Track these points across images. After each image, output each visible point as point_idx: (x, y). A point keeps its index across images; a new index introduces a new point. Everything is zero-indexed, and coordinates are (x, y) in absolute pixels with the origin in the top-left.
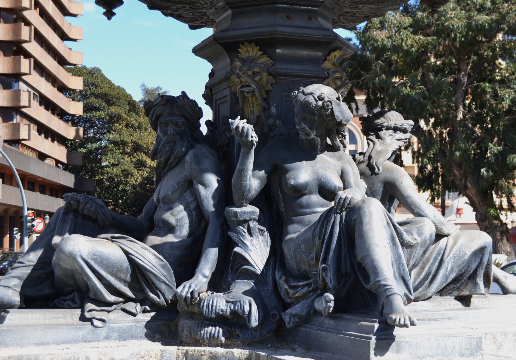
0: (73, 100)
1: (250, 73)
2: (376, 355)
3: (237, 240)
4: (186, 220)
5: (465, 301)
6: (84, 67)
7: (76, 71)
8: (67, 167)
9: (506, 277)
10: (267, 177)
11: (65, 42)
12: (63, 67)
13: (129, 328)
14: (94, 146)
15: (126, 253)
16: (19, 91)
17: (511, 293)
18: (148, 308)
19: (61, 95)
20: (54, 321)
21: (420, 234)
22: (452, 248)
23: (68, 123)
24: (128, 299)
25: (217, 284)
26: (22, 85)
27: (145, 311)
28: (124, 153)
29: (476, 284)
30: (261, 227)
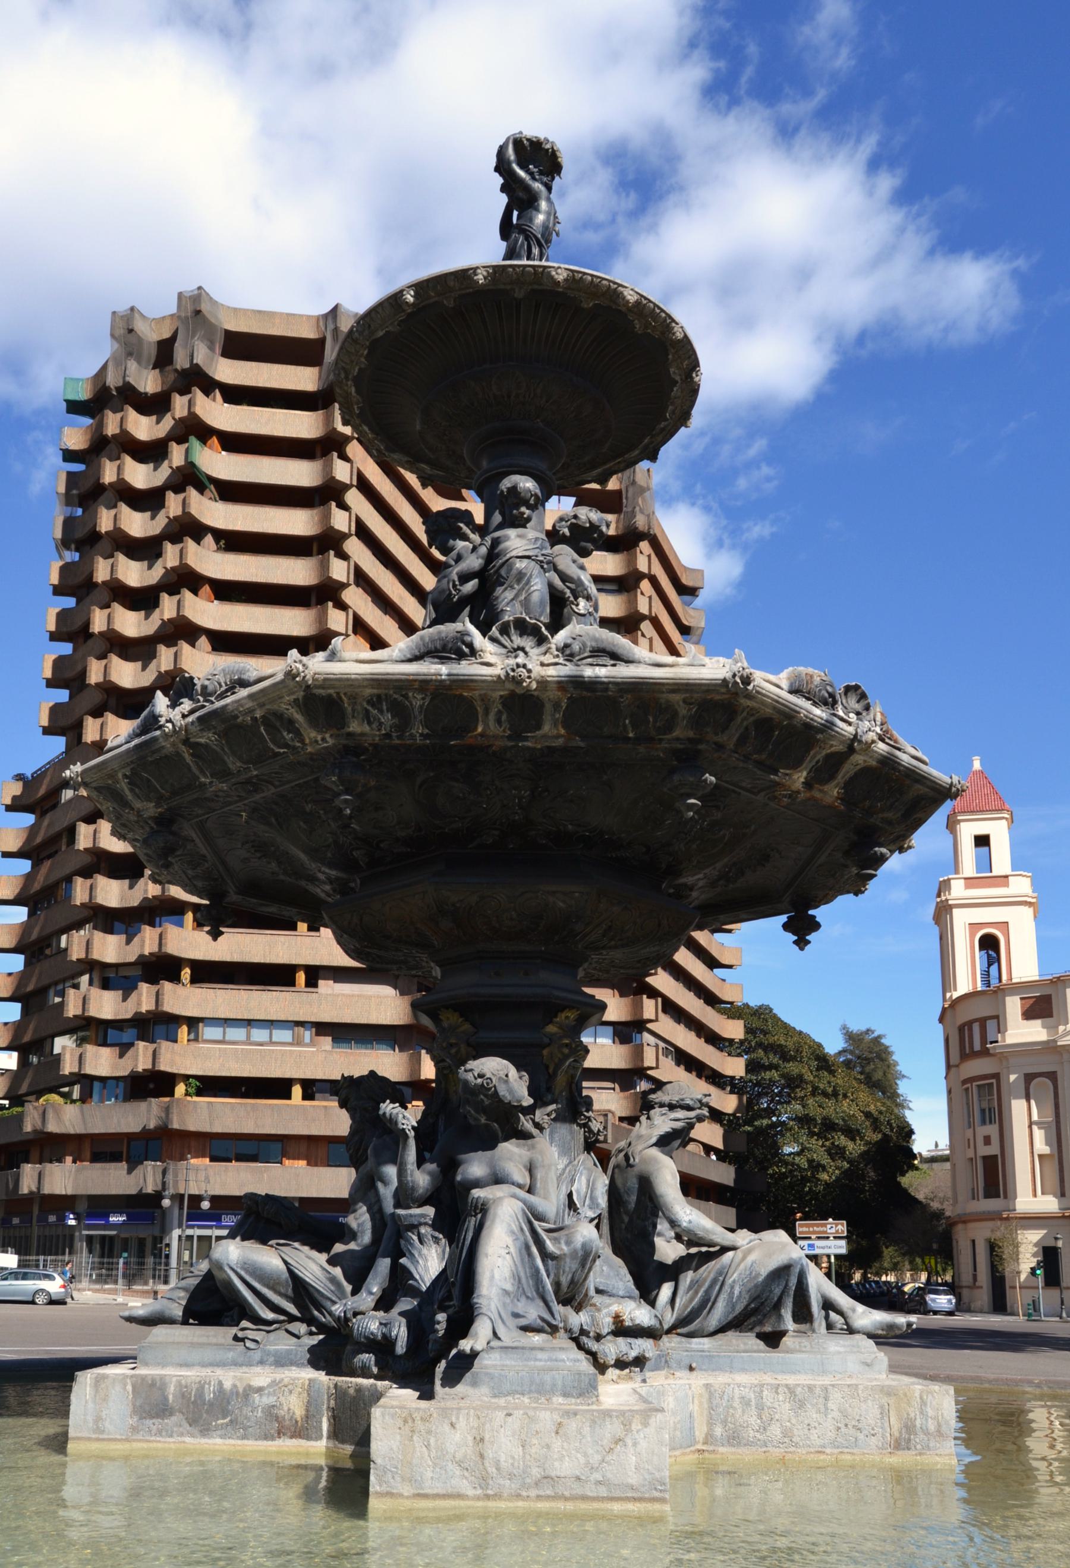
1: (444, 1045)
2: (443, 1386)
3: (405, 1249)
4: (368, 1225)
5: (773, 1340)
6: (747, 1005)
7: (733, 1011)
8: (723, 1156)
9: (854, 1310)
10: (441, 1171)
11: (715, 970)
12: (713, 1007)
13: (289, 1352)
14: (765, 1122)
15: (286, 1262)
16: (642, 1045)
17: (859, 1332)
18: (314, 1329)
21: (568, 1243)
22: (739, 1265)
23: (724, 1089)
24: (292, 1319)
25: (384, 1303)
26: (647, 1037)
27: (311, 1333)
28: (812, 1134)
29: (780, 1317)
30: (437, 1234)
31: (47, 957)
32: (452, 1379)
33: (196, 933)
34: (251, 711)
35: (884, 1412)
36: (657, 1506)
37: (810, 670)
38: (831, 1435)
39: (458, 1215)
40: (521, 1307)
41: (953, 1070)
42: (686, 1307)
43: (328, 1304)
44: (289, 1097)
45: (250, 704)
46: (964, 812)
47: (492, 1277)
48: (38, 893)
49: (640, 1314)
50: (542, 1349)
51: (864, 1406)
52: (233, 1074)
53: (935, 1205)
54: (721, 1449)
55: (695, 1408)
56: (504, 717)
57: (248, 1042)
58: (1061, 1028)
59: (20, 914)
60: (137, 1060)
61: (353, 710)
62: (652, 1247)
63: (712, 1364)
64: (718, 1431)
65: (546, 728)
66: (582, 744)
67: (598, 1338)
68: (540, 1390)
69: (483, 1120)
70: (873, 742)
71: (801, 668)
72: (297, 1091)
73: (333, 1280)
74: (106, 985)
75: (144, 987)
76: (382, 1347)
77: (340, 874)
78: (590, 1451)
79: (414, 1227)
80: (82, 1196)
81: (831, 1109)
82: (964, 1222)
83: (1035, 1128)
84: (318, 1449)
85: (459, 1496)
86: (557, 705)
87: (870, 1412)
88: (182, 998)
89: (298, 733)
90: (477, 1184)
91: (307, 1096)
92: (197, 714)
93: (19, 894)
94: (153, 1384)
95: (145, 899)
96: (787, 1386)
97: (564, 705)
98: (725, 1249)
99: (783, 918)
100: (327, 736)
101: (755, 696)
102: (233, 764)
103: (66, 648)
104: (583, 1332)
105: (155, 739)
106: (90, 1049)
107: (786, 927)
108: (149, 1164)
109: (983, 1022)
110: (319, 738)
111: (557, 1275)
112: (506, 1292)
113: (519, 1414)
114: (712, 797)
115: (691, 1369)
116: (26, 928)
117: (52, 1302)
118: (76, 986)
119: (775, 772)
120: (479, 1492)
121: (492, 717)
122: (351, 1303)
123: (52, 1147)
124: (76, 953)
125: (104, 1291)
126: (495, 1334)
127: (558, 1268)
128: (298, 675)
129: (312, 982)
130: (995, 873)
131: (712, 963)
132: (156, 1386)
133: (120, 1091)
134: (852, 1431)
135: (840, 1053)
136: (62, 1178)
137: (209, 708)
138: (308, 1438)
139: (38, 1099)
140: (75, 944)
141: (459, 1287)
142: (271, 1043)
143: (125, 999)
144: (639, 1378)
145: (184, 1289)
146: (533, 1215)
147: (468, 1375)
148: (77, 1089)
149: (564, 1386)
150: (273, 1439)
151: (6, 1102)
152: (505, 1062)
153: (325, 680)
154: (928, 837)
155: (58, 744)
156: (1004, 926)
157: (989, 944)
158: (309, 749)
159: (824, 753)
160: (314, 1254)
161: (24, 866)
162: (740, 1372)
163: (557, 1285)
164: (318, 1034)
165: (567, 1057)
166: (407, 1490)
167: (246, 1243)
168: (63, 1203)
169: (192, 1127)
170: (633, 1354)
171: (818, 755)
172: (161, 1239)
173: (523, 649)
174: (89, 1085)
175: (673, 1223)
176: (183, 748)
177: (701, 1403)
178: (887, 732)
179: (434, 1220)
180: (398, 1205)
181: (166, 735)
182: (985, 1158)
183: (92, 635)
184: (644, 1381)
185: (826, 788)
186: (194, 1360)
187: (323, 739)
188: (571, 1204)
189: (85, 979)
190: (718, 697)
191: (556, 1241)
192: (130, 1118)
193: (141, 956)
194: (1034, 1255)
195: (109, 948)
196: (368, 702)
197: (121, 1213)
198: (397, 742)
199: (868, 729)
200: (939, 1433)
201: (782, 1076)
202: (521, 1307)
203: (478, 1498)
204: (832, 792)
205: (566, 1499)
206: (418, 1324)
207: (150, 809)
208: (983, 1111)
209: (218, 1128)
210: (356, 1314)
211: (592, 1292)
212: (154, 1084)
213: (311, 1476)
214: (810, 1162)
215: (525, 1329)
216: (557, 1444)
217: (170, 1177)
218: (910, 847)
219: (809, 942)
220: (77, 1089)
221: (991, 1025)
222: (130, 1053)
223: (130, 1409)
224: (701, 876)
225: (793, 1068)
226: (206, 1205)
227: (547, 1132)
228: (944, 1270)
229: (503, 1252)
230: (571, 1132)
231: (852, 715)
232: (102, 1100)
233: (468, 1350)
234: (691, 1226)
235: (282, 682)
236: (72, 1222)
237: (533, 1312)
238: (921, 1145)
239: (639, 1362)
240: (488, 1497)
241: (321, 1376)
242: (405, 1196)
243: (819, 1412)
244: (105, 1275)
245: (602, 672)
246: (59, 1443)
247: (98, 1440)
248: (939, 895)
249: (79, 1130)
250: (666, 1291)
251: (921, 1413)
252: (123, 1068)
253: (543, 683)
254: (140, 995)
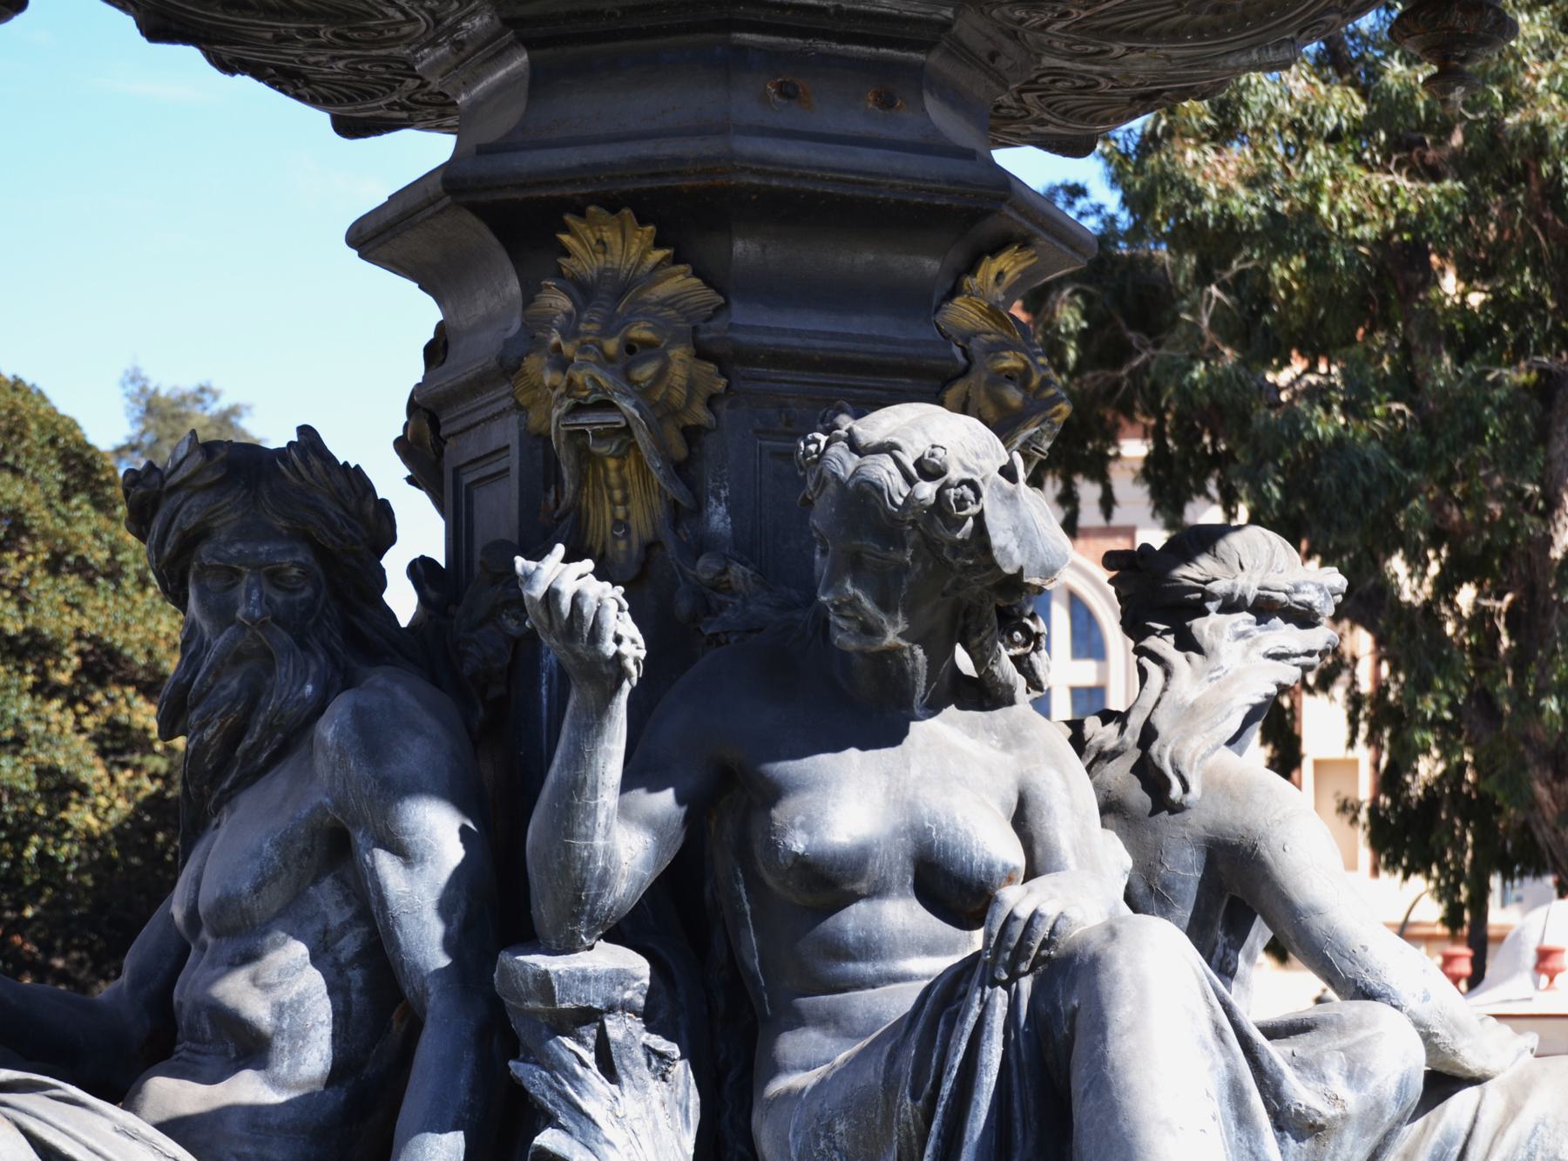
1: (612, 346)
3: (548, 1099)
4: (320, 1011)
10: (687, 818)
21: (1355, 1074)
28: (44, 689)
135: (119, 452)
179: (651, 995)
214: (44, 772)
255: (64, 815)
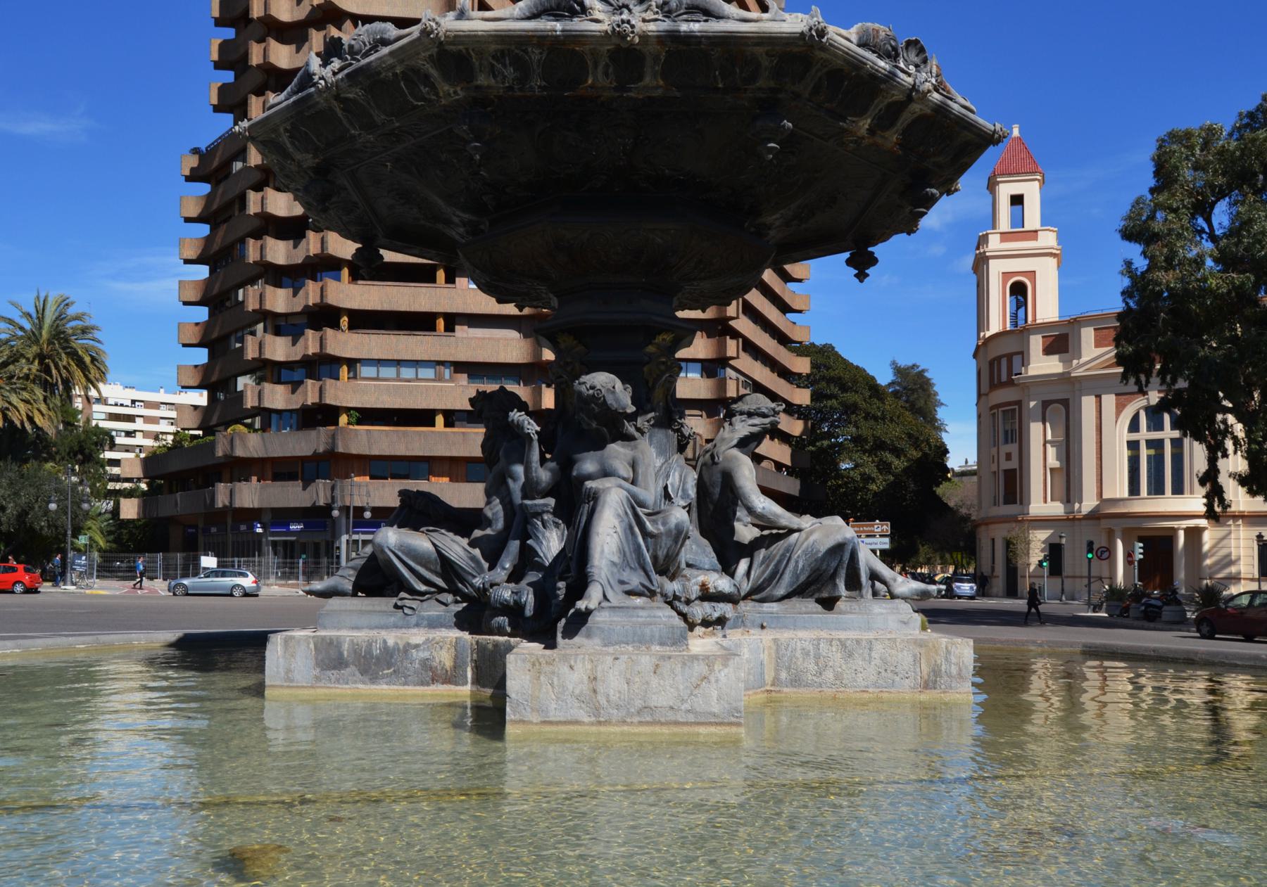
0: (798, 387)
2: (563, 638)
4: (501, 514)
5: (829, 604)
6: (813, 344)
7: (802, 350)
8: (792, 471)
9: (895, 580)
19: (782, 381)
20: (370, 608)
21: (664, 524)
25: (515, 577)
26: (730, 372)
27: (457, 602)
28: (865, 452)
29: (835, 585)
31: (228, 308)
32: (570, 633)
33: (352, 286)
34: (392, 67)
35: (916, 660)
36: (734, 729)
37: (877, 26)
38: (873, 678)
39: (575, 504)
40: (626, 575)
41: (983, 398)
42: (759, 578)
43: (470, 578)
44: (433, 425)
45: (391, 61)
46: (1002, 175)
47: (603, 551)
48: (217, 253)
49: (722, 583)
50: (643, 608)
51: (900, 655)
52: (386, 406)
53: (964, 511)
54: (785, 690)
55: (765, 657)
56: (611, 70)
57: (398, 379)
58: (1075, 362)
59: (203, 272)
60: (306, 395)
61: (481, 65)
62: (732, 531)
63: (779, 622)
64: (784, 675)
65: (647, 80)
66: (678, 94)
67: (688, 602)
68: (641, 640)
69: (594, 425)
70: (929, 91)
71: (869, 24)
72: (440, 420)
73: (473, 558)
74: (278, 332)
75: (310, 333)
76: (514, 611)
77: (474, 218)
78: (681, 687)
79: (538, 515)
80: (266, 509)
81: (880, 430)
82: (987, 524)
83: (1048, 446)
84: (464, 691)
85: (577, 722)
86: (656, 58)
87: (905, 659)
88: (343, 342)
89: (433, 87)
90: (590, 477)
91: (448, 424)
92: (346, 71)
93: (201, 254)
94: (331, 643)
95: (308, 257)
96: (839, 640)
97: (663, 58)
98: (791, 531)
99: (847, 255)
100: (458, 89)
101: (830, 48)
102: (379, 117)
103: (230, 33)
104: (676, 597)
105: (310, 96)
106: (267, 386)
107: (849, 262)
108: (320, 482)
109: (1010, 357)
110: (451, 91)
111: (655, 550)
112: (614, 564)
113: (624, 658)
114: (789, 142)
115: (763, 627)
116: (208, 283)
117: (246, 595)
118: (253, 333)
119: (844, 119)
120: (593, 719)
121: (600, 69)
122: (488, 576)
123: (240, 469)
124: (252, 305)
125: (289, 586)
126: (605, 596)
127: (656, 545)
128: (432, 32)
129: (450, 328)
130: (1027, 228)
131: (785, 308)
132: (333, 644)
133: (294, 421)
134: (890, 675)
135: (890, 385)
136: (249, 494)
137: (356, 65)
138: (456, 684)
139: (226, 429)
140: (250, 297)
141: (576, 562)
142: (417, 379)
143: (294, 344)
144: (720, 634)
145: (352, 568)
146: (635, 503)
147: (584, 629)
148: (258, 419)
149: (660, 637)
150: (428, 685)
151: (200, 432)
152: (612, 376)
153: (456, 36)
154: (971, 181)
155: (225, 122)
156: (1032, 274)
157: (1019, 291)
158: (443, 102)
159: (886, 102)
160: (458, 538)
161: (204, 230)
162: (801, 632)
163: (655, 558)
164: (455, 372)
165: (663, 373)
166: (535, 718)
167: (402, 530)
168: (252, 515)
169: (354, 450)
170: (716, 615)
171: (880, 104)
172: (333, 543)
173: (627, 7)
174: (268, 417)
175: (751, 511)
176: (335, 103)
177: (770, 654)
178: (941, 83)
179: (555, 509)
180: (525, 497)
181: (319, 91)
182: (1006, 471)
183: (252, 20)
184: (725, 636)
185: (887, 134)
186: (362, 624)
187: (455, 92)
188: (667, 496)
189: (260, 327)
190: (796, 50)
191: (654, 522)
192: (303, 444)
193: (307, 307)
194: (1042, 551)
195: (279, 300)
196: (493, 57)
197: (299, 523)
198: (519, 93)
199: (925, 79)
200: (960, 676)
201: (840, 403)
202: (626, 575)
203: (592, 724)
204: (893, 137)
205: (662, 724)
206: (543, 592)
207: (308, 160)
208: (1006, 432)
209: (375, 452)
210: (492, 585)
211: (683, 565)
212: (323, 415)
213: (459, 710)
215: (630, 593)
216: (654, 681)
217: (338, 492)
218: (956, 190)
219: (867, 275)
220: (258, 419)
221: (1017, 360)
222: (300, 390)
223: (313, 662)
224: (777, 216)
225: (850, 397)
226: (368, 515)
227: (647, 435)
228: (968, 564)
229: (611, 531)
230: (667, 436)
231: (911, 67)
232: (279, 430)
233: (583, 607)
234: (765, 512)
235: (418, 39)
236: (259, 530)
237: (636, 580)
238: (955, 462)
239: (721, 621)
240: (600, 723)
241: (466, 635)
242: (531, 489)
243: (864, 660)
244: (288, 573)
245: (696, 27)
246: (258, 690)
247: (288, 687)
248: (978, 248)
249: (261, 454)
250: (743, 565)
251: (946, 660)
252: (296, 354)
253: (644, 37)
254: (307, 340)
255: (126, 462)
